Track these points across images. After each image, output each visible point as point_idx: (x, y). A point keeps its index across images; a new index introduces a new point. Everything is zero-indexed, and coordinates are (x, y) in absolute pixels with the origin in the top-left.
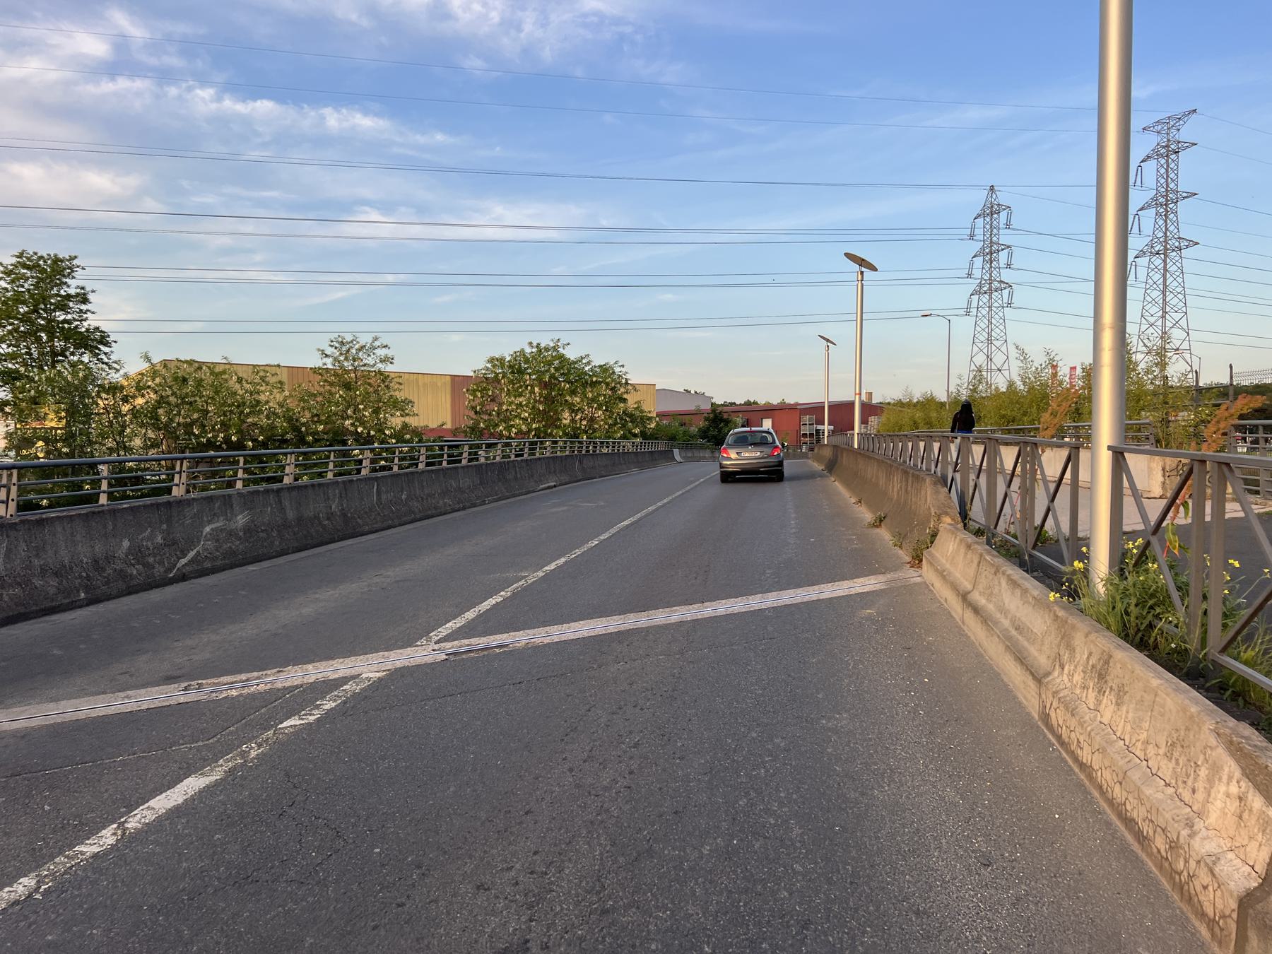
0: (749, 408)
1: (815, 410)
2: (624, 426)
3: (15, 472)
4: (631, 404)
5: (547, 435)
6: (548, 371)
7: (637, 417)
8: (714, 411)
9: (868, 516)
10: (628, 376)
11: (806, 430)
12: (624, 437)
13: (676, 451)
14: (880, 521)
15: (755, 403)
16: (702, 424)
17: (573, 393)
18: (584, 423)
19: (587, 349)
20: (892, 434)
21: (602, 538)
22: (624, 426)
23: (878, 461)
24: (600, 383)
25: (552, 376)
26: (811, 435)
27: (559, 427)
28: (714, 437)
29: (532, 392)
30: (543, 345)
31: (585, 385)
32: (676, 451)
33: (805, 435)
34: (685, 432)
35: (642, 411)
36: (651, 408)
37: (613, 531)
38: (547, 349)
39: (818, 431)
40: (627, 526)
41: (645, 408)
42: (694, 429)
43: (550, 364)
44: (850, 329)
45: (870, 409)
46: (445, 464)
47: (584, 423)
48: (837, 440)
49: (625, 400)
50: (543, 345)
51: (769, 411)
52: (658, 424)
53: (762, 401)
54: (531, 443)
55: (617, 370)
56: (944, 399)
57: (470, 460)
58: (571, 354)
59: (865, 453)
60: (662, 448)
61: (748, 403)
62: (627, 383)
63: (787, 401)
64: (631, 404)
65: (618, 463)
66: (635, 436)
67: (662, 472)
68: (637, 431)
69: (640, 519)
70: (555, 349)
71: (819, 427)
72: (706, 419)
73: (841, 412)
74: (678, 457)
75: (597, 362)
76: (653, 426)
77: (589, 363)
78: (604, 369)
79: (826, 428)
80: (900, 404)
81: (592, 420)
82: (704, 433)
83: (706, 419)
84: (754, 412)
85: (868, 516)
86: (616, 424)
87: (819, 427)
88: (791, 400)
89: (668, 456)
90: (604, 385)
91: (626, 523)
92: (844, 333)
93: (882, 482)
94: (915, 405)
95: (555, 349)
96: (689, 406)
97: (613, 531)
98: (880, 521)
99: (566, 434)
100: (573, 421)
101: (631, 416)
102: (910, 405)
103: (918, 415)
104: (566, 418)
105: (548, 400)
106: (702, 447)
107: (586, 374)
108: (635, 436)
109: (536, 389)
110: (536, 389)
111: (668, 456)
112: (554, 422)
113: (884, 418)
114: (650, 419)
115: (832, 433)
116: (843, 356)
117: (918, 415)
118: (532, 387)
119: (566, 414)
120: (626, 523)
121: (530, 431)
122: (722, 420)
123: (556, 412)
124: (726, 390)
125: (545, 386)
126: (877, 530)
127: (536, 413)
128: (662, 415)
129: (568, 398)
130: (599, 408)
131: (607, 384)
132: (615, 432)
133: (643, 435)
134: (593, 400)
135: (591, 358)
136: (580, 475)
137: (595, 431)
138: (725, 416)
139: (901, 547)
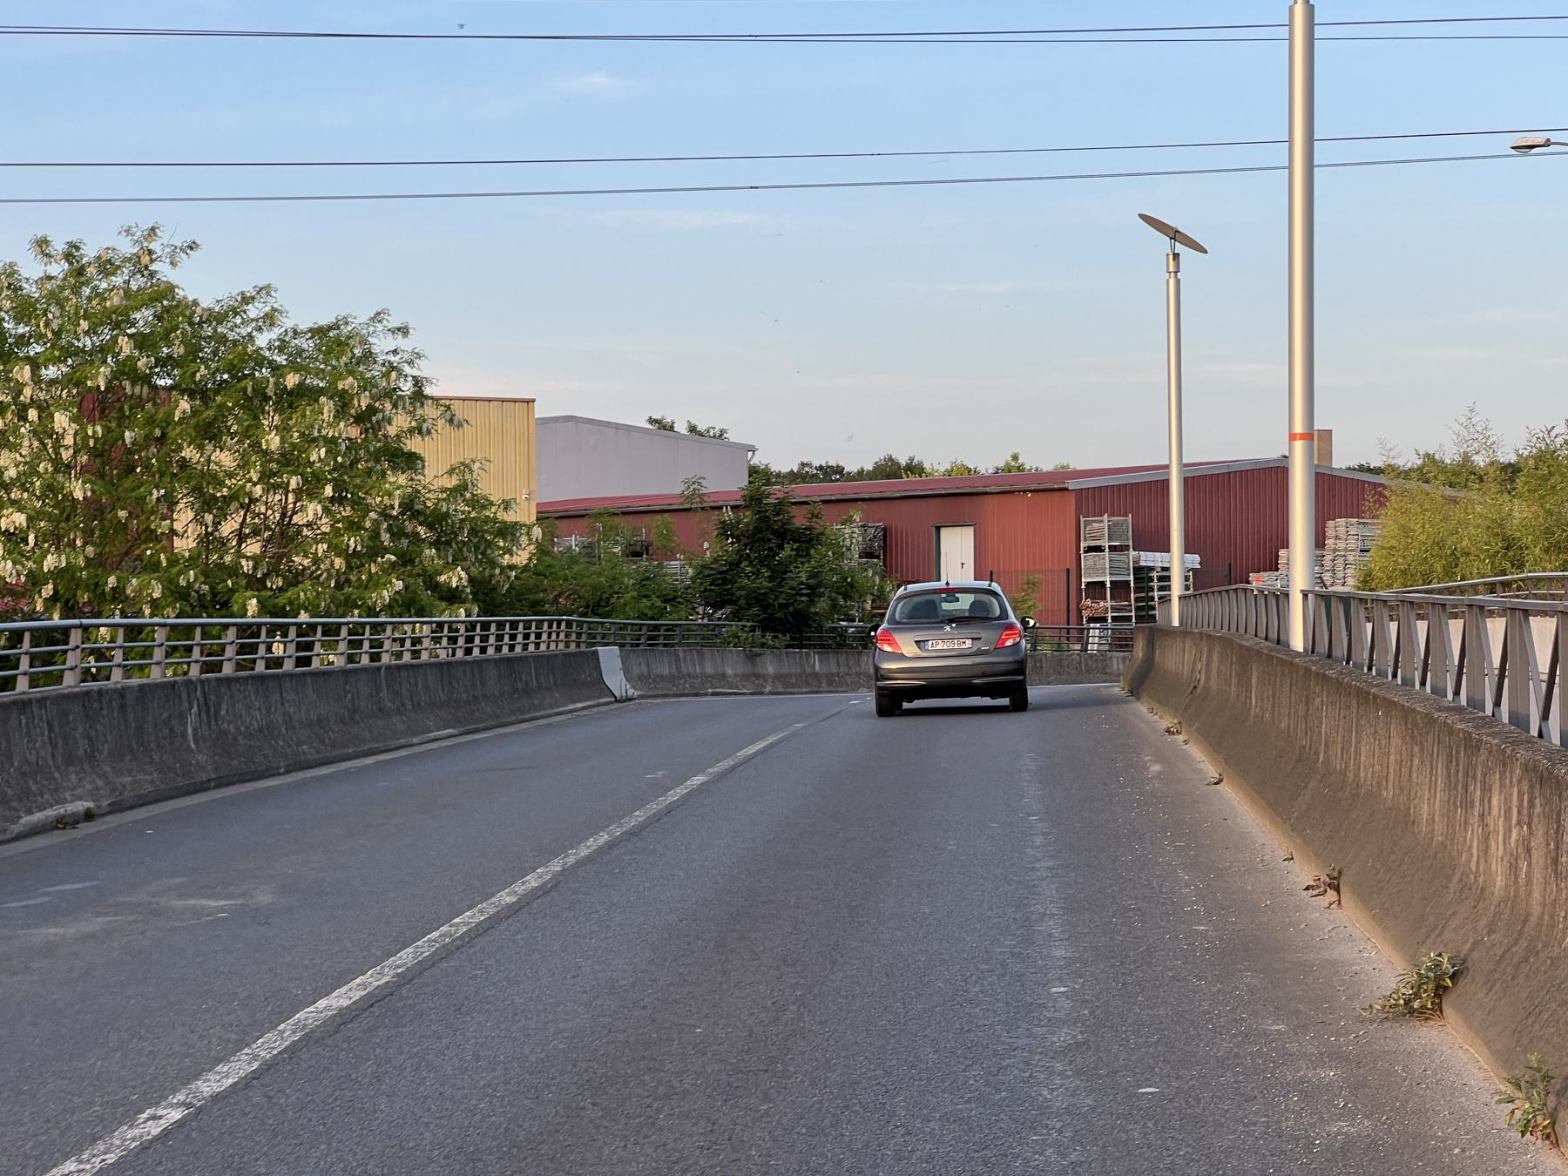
0: (908, 482)
1: (1135, 497)
2: (406, 559)
3: (121, 632)
4: (435, 477)
5: (102, 601)
6: (104, 350)
7: (463, 528)
8: (753, 499)
9: (1379, 963)
10: (422, 369)
11: (1098, 570)
12: (407, 604)
13: (610, 657)
14: (1434, 993)
15: (914, 468)
16: (709, 549)
17: (209, 433)
18: (253, 548)
19: (264, 263)
20: (1434, 585)
21: (211, 1085)
22: (406, 559)
23: (1407, 713)
24: (313, 394)
25: (126, 370)
26: (1120, 588)
27: (153, 566)
28: (759, 599)
29: (44, 431)
30: (89, 252)
31: (255, 402)
32: (610, 657)
33: (1096, 589)
34: (644, 580)
35: (480, 503)
36: (517, 489)
37: (270, 1045)
38: (107, 266)
39: (1142, 573)
40: (345, 1017)
41: (487, 487)
42: (679, 570)
43: (119, 319)
44: (1266, 202)
45: (1342, 494)
46: (22, 684)
47: (253, 548)
48: (1219, 610)
49: (411, 461)
50: (89, 252)
51: (961, 497)
52: (542, 550)
53: (938, 459)
54: (243, 630)
55: (382, 345)
56: (1420, 462)
57: (240, 666)
58: (201, 284)
59: (1331, 674)
60: (552, 644)
61: (889, 469)
62: (419, 396)
63: (1030, 462)
64: (435, 477)
65: (372, 710)
66: (452, 597)
67: (547, 757)
68: (456, 578)
69: (406, 979)
70: (140, 263)
71: (1149, 559)
72: (725, 530)
73: (1236, 512)
74: (616, 681)
75: (304, 312)
76: (521, 557)
77: (270, 319)
78: (331, 339)
79: (1177, 561)
80: (1429, 470)
81: (285, 536)
82: (719, 587)
83: (725, 530)
84: (910, 504)
85: (1379, 963)
86: (374, 551)
87: (1149, 559)
88: (1042, 458)
89: (577, 675)
90: (343, 400)
91: (339, 999)
92: (1242, 214)
93: (1429, 806)
94: (1511, 471)
95: (140, 263)
96: (660, 481)
97: (270, 1045)
98: (1434, 993)
99: (177, 594)
100: (209, 541)
101: (435, 520)
102: (1462, 475)
103: (1520, 512)
104: (186, 527)
105: (106, 461)
106: (710, 638)
107: (260, 361)
108: (452, 597)
109: (61, 420)
110: (61, 420)
111: (577, 675)
112: (124, 539)
113: (1383, 528)
114: (509, 531)
115: (1200, 581)
116: (1238, 300)
117: (1520, 512)
118: (44, 409)
119: (184, 517)
120: (339, 999)
121: (36, 580)
122: (785, 534)
123: (139, 507)
124: (806, 415)
125: (93, 406)
126: (1425, 1035)
127: (60, 518)
128: (555, 517)
129: (189, 452)
130: (310, 490)
131: (344, 402)
132: (374, 583)
133: (485, 594)
134: (289, 459)
135: (280, 299)
136: (203, 761)
137: (295, 578)
138: (800, 520)
139: (1553, 1139)
